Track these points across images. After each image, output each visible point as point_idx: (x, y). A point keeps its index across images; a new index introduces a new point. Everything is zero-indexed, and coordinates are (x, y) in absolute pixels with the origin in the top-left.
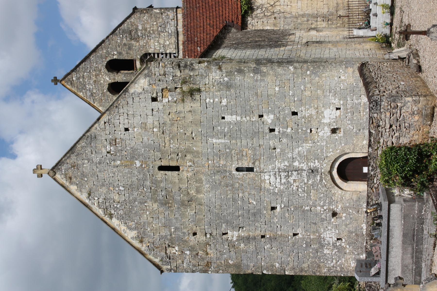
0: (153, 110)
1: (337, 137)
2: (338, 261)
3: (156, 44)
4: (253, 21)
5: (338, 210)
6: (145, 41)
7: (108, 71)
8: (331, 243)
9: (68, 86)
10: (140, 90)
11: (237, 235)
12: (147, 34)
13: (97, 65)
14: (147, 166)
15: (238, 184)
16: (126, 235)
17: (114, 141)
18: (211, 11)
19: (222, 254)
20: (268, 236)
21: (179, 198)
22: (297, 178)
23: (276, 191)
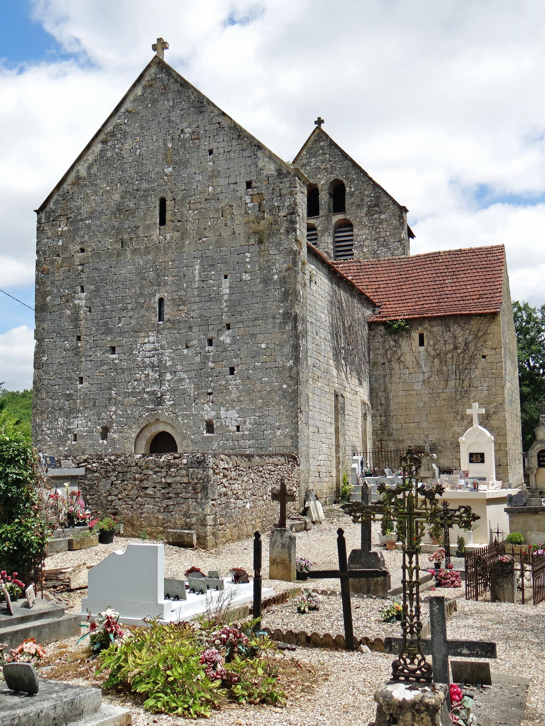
0: (236, 183)
1: (202, 429)
2: (49, 437)
3: (364, 237)
4: (380, 337)
5: (111, 433)
6: (367, 223)
7: (331, 183)
8: (71, 427)
9: (313, 137)
10: (260, 164)
11: (80, 304)
12: (376, 226)
13: (337, 169)
14: (165, 182)
15: (143, 301)
16: (82, 163)
17: (196, 136)
18: (395, 288)
19: (58, 287)
20: (79, 344)
21: (127, 227)
22: (150, 378)
23: (134, 352)
